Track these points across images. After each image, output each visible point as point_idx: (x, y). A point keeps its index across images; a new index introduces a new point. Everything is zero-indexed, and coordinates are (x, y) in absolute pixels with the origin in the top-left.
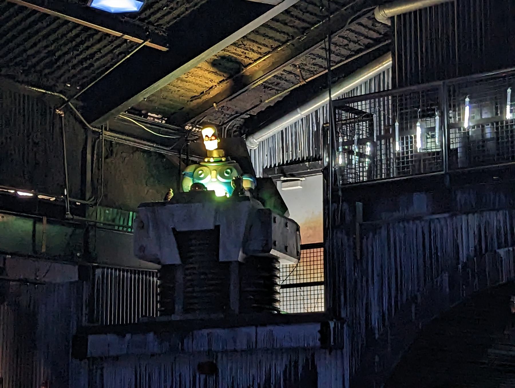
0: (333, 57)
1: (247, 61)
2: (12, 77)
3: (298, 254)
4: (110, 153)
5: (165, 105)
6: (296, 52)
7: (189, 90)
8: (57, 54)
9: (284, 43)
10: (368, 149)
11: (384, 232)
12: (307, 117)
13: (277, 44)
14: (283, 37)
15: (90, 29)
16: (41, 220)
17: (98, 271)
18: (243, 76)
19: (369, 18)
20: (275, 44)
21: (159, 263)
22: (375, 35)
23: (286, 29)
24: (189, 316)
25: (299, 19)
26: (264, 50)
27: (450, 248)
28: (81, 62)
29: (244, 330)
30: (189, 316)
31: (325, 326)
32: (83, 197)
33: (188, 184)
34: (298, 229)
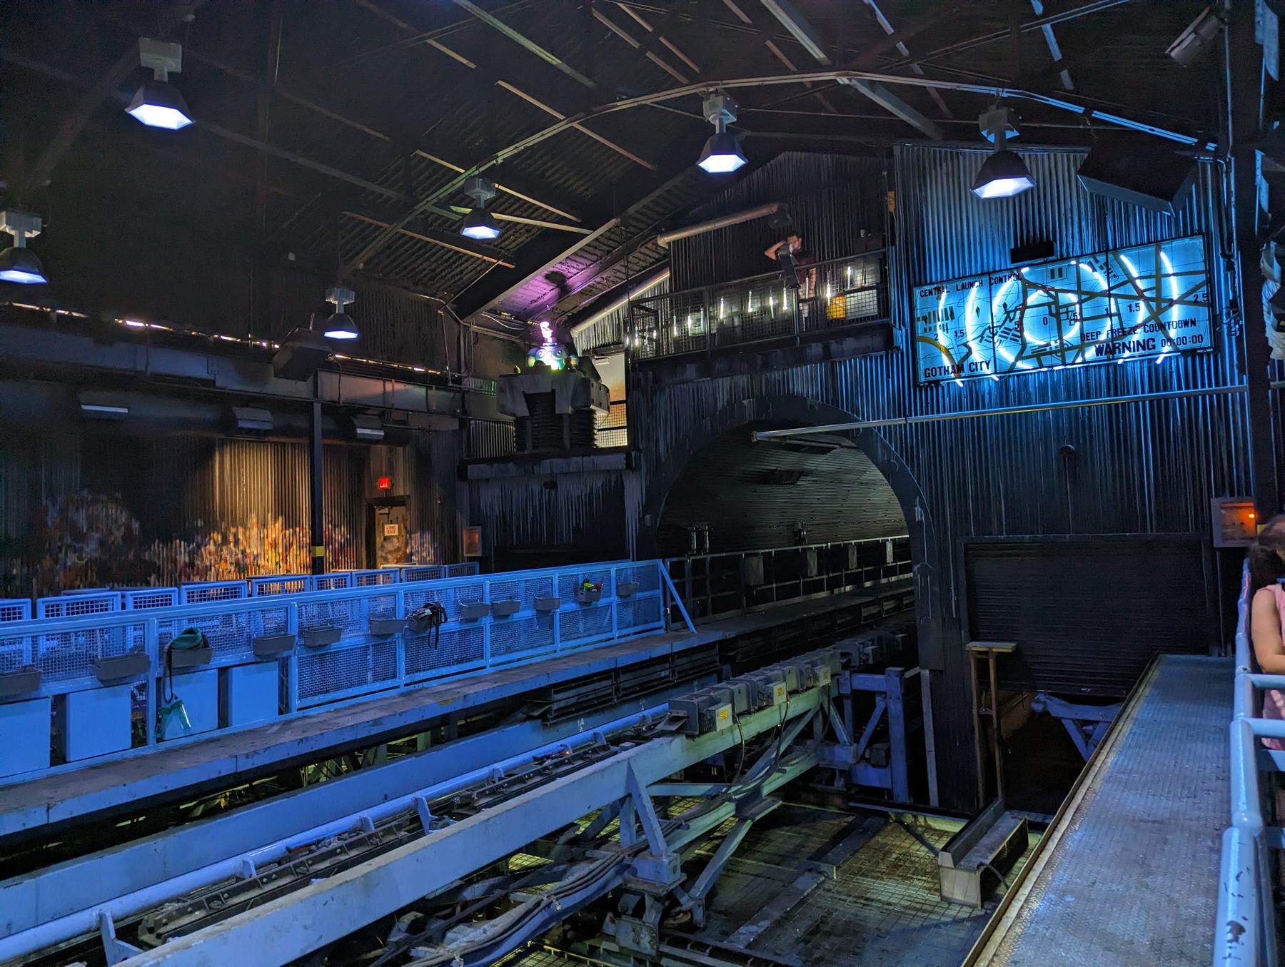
0: (630, 273)
1: (569, 275)
2: (405, 288)
3: (609, 408)
4: (476, 341)
5: (513, 307)
6: (603, 269)
7: (531, 296)
8: (437, 271)
9: (595, 262)
10: (655, 334)
11: (667, 391)
12: (612, 314)
13: (590, 262)
14: (595, 258)
15: (459, 252)
16: (431, 388)
17: (472, 422)
18: (566, 286)
19: (653, 244)
20: (589, 263)
21: (514, 415)
22: (657, 256)
23: (597, 252)
24: (537, 451)
25: (605, 245)
26: (581, 267)
27: (711, 399)
28: (453, 277)
29: (574, 459)
30: (537, 451)
31: (629, 455)
32: (460, 372)
33: (532, 362)
34: (608, 391)
